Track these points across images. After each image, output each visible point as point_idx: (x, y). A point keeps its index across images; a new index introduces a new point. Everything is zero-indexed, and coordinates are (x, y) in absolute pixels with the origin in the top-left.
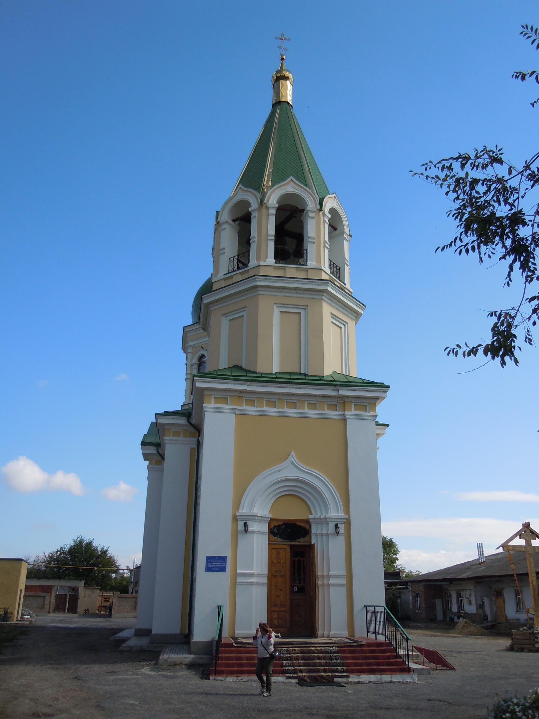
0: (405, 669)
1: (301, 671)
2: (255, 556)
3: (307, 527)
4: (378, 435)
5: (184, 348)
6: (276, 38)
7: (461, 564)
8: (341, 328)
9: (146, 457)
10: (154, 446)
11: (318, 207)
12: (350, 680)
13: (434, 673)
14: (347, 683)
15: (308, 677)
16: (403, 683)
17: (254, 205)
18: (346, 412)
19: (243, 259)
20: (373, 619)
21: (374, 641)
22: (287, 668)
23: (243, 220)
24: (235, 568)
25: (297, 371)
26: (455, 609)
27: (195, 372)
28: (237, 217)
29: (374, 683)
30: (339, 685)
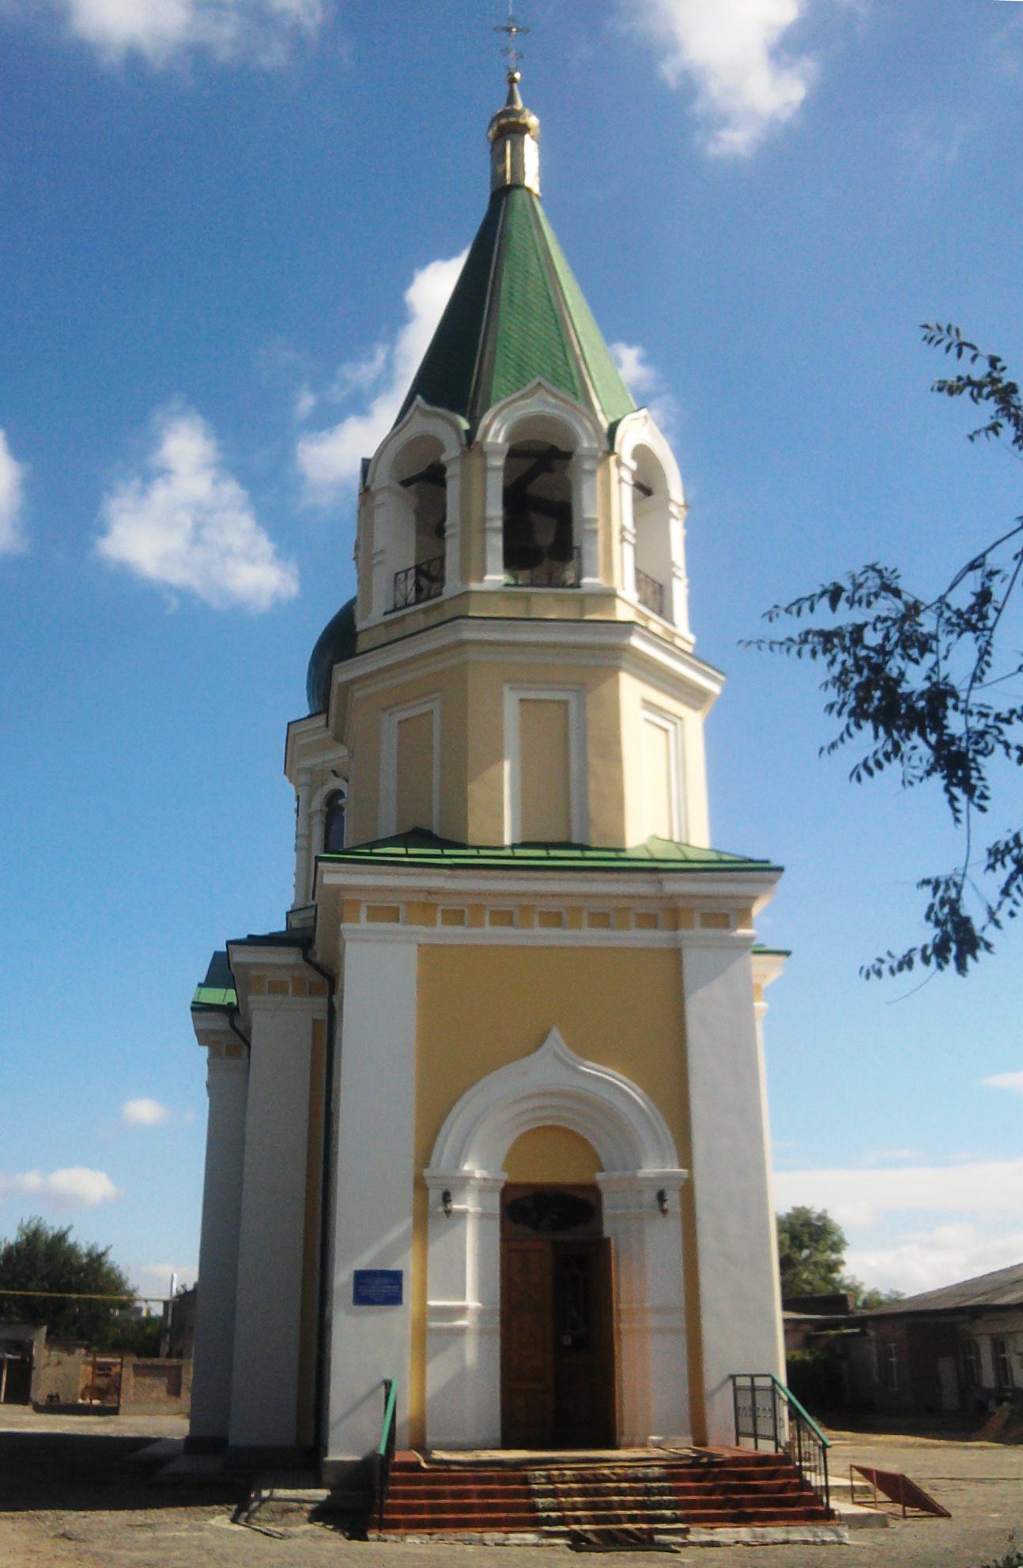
1: (578, 1520)
2: (463, 1278)
7: (1001, 1271)
8: (666, 731)
9: (203, 1036)
10: (226, 1031)
11: (605, 446)
12: (691, 1538)
13: (896, 1525)
14: (683, 1545)
15: (594, 1532)
16: (814, 1543)
17: (451, 453)
18: (682, 933)
19: (428, 575)
20: (749, 1403)
22: (544, 1514)
24: (423, 1297)
25: (560, 837)
26: (988, 1379)
27: (317, 850)
28: (414, 473)
29: (747, 1544)
30: (665, 1548)
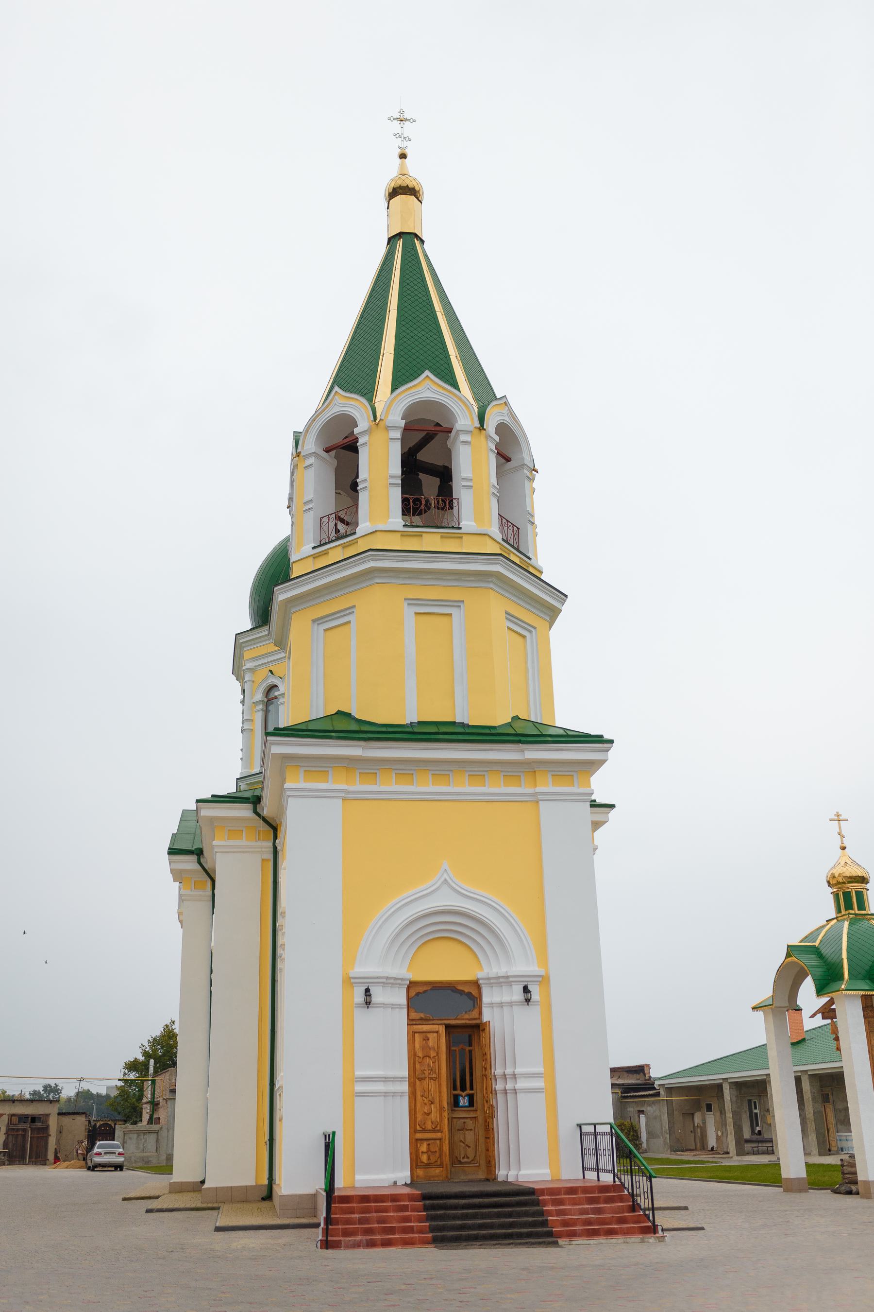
0: (648, 1227)
2: (386, 1044)
3: (475, 993)
4: (596, 825)
5: (238, 671)
6: (389, 119)
9: (178, 875)
11: (478, 425)
17: (363, 424)
19: (343, 520)
21: (596, 1184)
23: (342, 448)
